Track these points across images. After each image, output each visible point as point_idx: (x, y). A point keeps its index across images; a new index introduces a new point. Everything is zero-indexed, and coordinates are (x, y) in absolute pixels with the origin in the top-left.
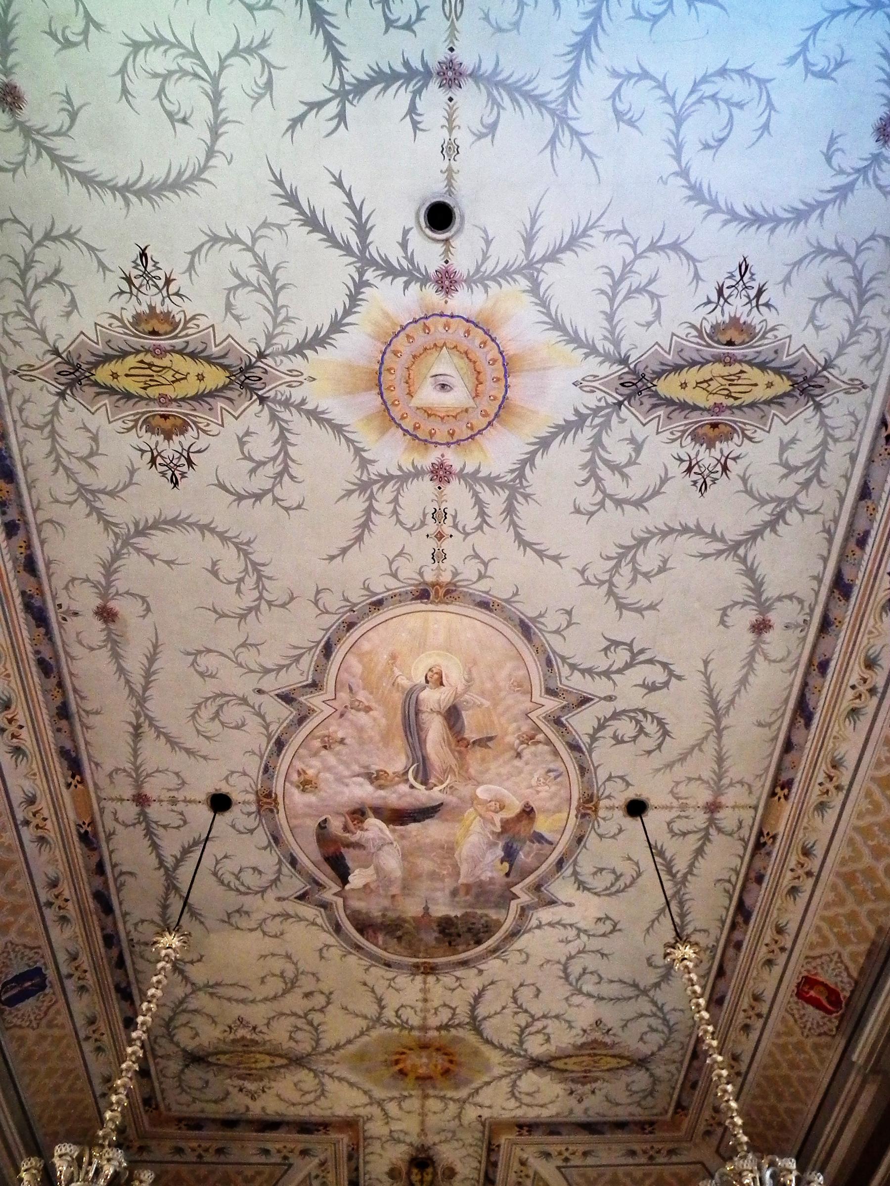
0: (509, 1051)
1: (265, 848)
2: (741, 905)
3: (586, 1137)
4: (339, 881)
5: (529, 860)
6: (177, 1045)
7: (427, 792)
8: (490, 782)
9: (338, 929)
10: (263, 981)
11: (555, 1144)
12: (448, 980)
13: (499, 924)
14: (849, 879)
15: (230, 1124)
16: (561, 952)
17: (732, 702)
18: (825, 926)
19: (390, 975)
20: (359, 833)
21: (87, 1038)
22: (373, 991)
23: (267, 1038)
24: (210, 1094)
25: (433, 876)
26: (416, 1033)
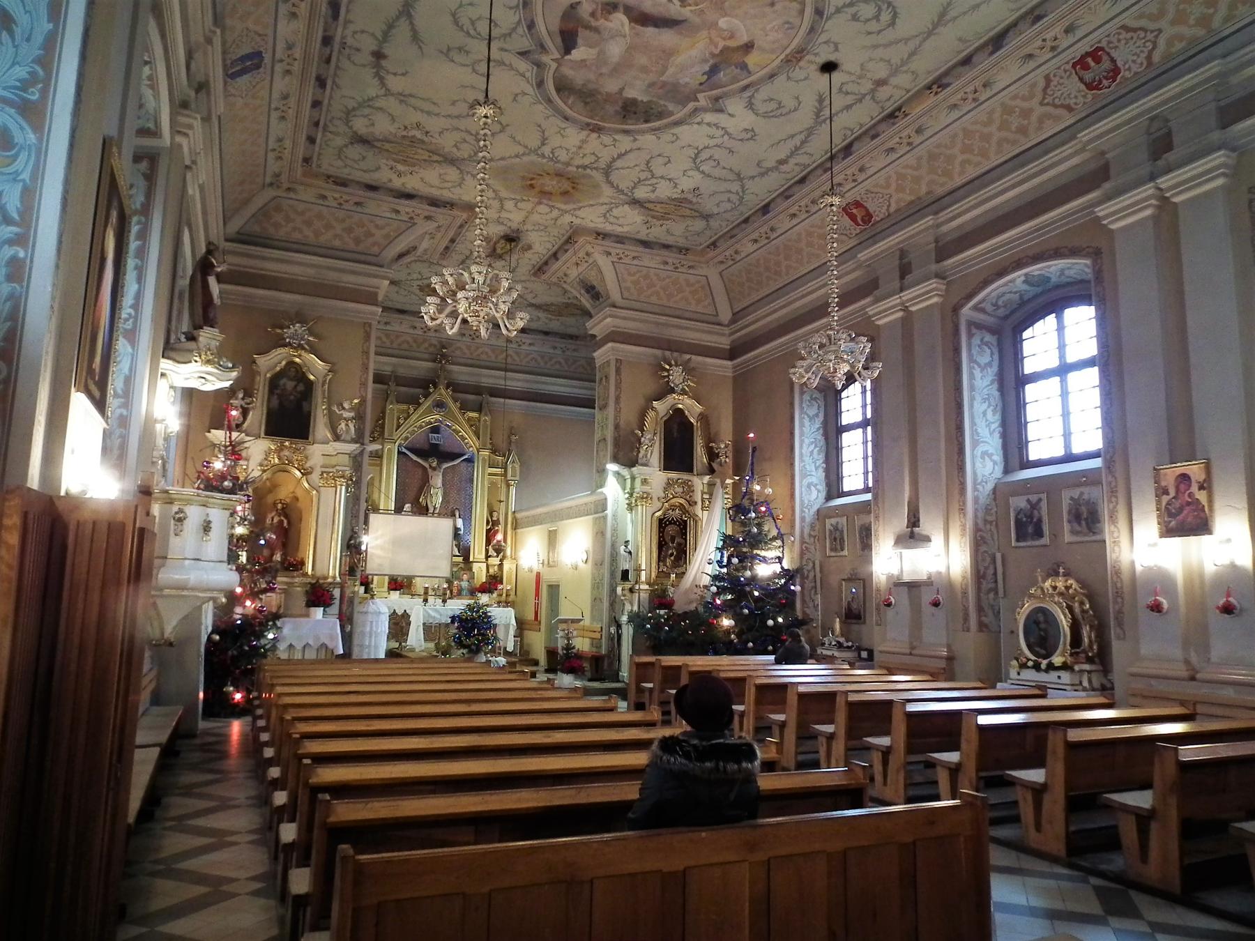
0: (622, 191)
1: (511, 8)
2: (850, 145)
3: (641, 249)
4: (563, 51)
5: (724, 79)
6: (351, 128)
7: (679, 8)
8: (736, 16)
9: (540, 84)
10: (454, 103)
11: (616, 249)
12: (606, 139)
13: (671, 114)
14: (932, 157)
15: (372, 188)
16: (702, 142)
17: (955, 18)
18: (894, 177)
19: (564, 125)
20: (602, 21)
21: (277, 109)
22: (543, 132)
23: (434, 141)
24: (363, 165)
25: (644, 69)
26: (559, 166)
